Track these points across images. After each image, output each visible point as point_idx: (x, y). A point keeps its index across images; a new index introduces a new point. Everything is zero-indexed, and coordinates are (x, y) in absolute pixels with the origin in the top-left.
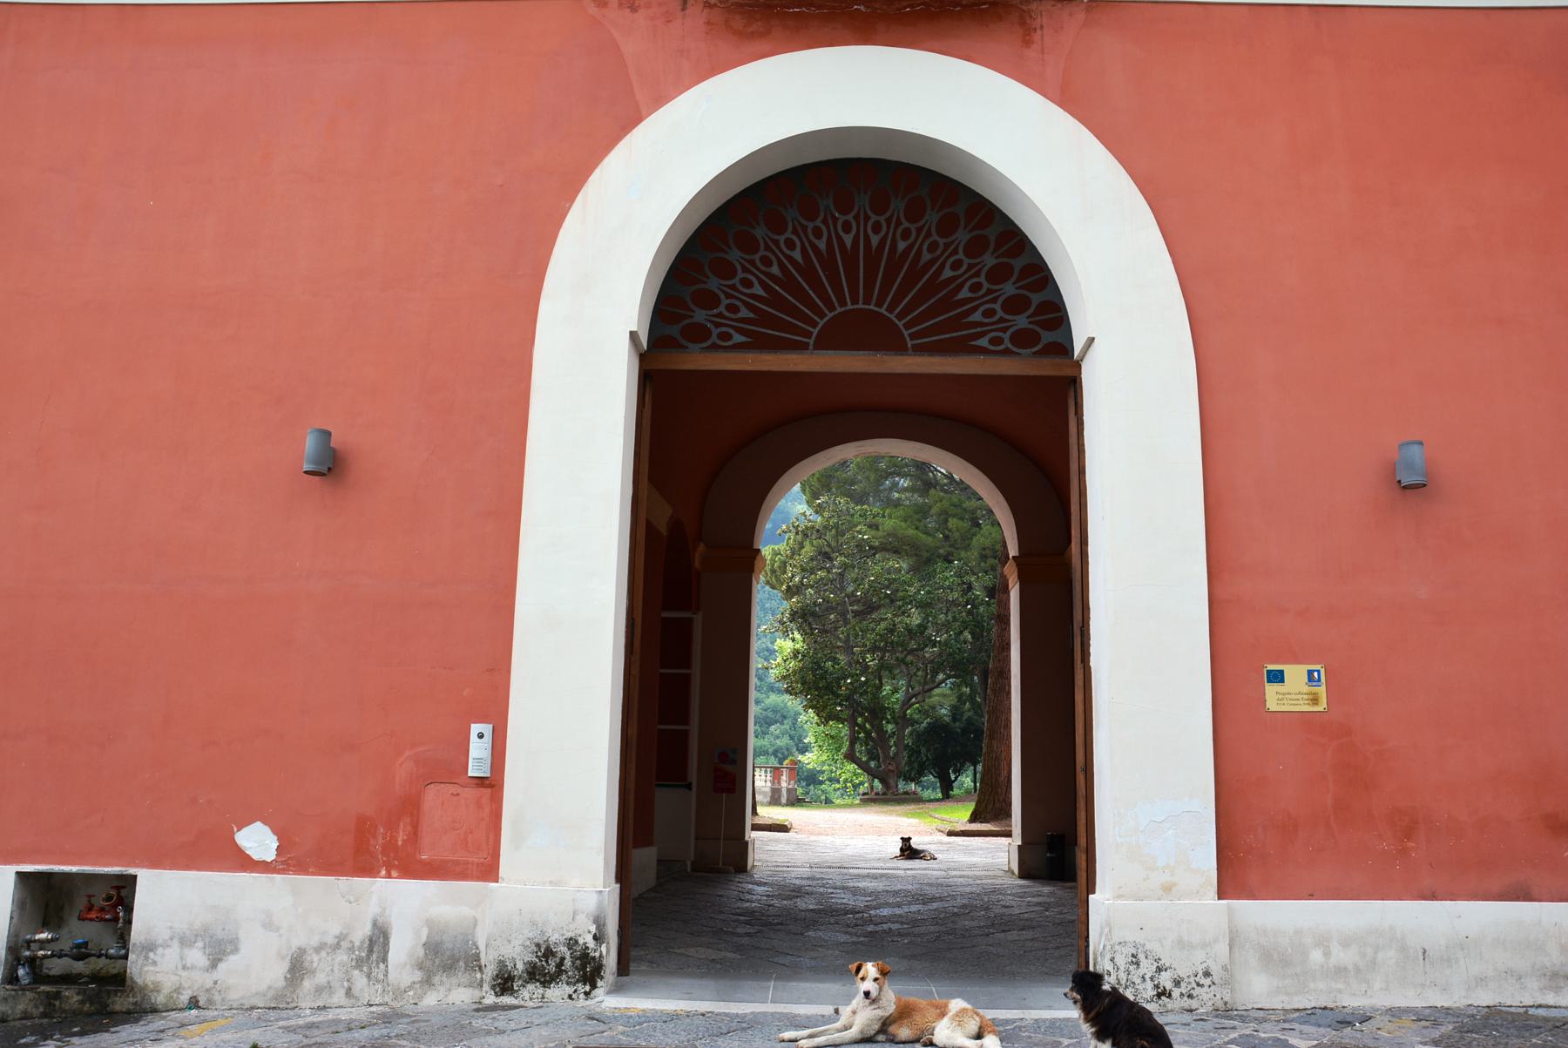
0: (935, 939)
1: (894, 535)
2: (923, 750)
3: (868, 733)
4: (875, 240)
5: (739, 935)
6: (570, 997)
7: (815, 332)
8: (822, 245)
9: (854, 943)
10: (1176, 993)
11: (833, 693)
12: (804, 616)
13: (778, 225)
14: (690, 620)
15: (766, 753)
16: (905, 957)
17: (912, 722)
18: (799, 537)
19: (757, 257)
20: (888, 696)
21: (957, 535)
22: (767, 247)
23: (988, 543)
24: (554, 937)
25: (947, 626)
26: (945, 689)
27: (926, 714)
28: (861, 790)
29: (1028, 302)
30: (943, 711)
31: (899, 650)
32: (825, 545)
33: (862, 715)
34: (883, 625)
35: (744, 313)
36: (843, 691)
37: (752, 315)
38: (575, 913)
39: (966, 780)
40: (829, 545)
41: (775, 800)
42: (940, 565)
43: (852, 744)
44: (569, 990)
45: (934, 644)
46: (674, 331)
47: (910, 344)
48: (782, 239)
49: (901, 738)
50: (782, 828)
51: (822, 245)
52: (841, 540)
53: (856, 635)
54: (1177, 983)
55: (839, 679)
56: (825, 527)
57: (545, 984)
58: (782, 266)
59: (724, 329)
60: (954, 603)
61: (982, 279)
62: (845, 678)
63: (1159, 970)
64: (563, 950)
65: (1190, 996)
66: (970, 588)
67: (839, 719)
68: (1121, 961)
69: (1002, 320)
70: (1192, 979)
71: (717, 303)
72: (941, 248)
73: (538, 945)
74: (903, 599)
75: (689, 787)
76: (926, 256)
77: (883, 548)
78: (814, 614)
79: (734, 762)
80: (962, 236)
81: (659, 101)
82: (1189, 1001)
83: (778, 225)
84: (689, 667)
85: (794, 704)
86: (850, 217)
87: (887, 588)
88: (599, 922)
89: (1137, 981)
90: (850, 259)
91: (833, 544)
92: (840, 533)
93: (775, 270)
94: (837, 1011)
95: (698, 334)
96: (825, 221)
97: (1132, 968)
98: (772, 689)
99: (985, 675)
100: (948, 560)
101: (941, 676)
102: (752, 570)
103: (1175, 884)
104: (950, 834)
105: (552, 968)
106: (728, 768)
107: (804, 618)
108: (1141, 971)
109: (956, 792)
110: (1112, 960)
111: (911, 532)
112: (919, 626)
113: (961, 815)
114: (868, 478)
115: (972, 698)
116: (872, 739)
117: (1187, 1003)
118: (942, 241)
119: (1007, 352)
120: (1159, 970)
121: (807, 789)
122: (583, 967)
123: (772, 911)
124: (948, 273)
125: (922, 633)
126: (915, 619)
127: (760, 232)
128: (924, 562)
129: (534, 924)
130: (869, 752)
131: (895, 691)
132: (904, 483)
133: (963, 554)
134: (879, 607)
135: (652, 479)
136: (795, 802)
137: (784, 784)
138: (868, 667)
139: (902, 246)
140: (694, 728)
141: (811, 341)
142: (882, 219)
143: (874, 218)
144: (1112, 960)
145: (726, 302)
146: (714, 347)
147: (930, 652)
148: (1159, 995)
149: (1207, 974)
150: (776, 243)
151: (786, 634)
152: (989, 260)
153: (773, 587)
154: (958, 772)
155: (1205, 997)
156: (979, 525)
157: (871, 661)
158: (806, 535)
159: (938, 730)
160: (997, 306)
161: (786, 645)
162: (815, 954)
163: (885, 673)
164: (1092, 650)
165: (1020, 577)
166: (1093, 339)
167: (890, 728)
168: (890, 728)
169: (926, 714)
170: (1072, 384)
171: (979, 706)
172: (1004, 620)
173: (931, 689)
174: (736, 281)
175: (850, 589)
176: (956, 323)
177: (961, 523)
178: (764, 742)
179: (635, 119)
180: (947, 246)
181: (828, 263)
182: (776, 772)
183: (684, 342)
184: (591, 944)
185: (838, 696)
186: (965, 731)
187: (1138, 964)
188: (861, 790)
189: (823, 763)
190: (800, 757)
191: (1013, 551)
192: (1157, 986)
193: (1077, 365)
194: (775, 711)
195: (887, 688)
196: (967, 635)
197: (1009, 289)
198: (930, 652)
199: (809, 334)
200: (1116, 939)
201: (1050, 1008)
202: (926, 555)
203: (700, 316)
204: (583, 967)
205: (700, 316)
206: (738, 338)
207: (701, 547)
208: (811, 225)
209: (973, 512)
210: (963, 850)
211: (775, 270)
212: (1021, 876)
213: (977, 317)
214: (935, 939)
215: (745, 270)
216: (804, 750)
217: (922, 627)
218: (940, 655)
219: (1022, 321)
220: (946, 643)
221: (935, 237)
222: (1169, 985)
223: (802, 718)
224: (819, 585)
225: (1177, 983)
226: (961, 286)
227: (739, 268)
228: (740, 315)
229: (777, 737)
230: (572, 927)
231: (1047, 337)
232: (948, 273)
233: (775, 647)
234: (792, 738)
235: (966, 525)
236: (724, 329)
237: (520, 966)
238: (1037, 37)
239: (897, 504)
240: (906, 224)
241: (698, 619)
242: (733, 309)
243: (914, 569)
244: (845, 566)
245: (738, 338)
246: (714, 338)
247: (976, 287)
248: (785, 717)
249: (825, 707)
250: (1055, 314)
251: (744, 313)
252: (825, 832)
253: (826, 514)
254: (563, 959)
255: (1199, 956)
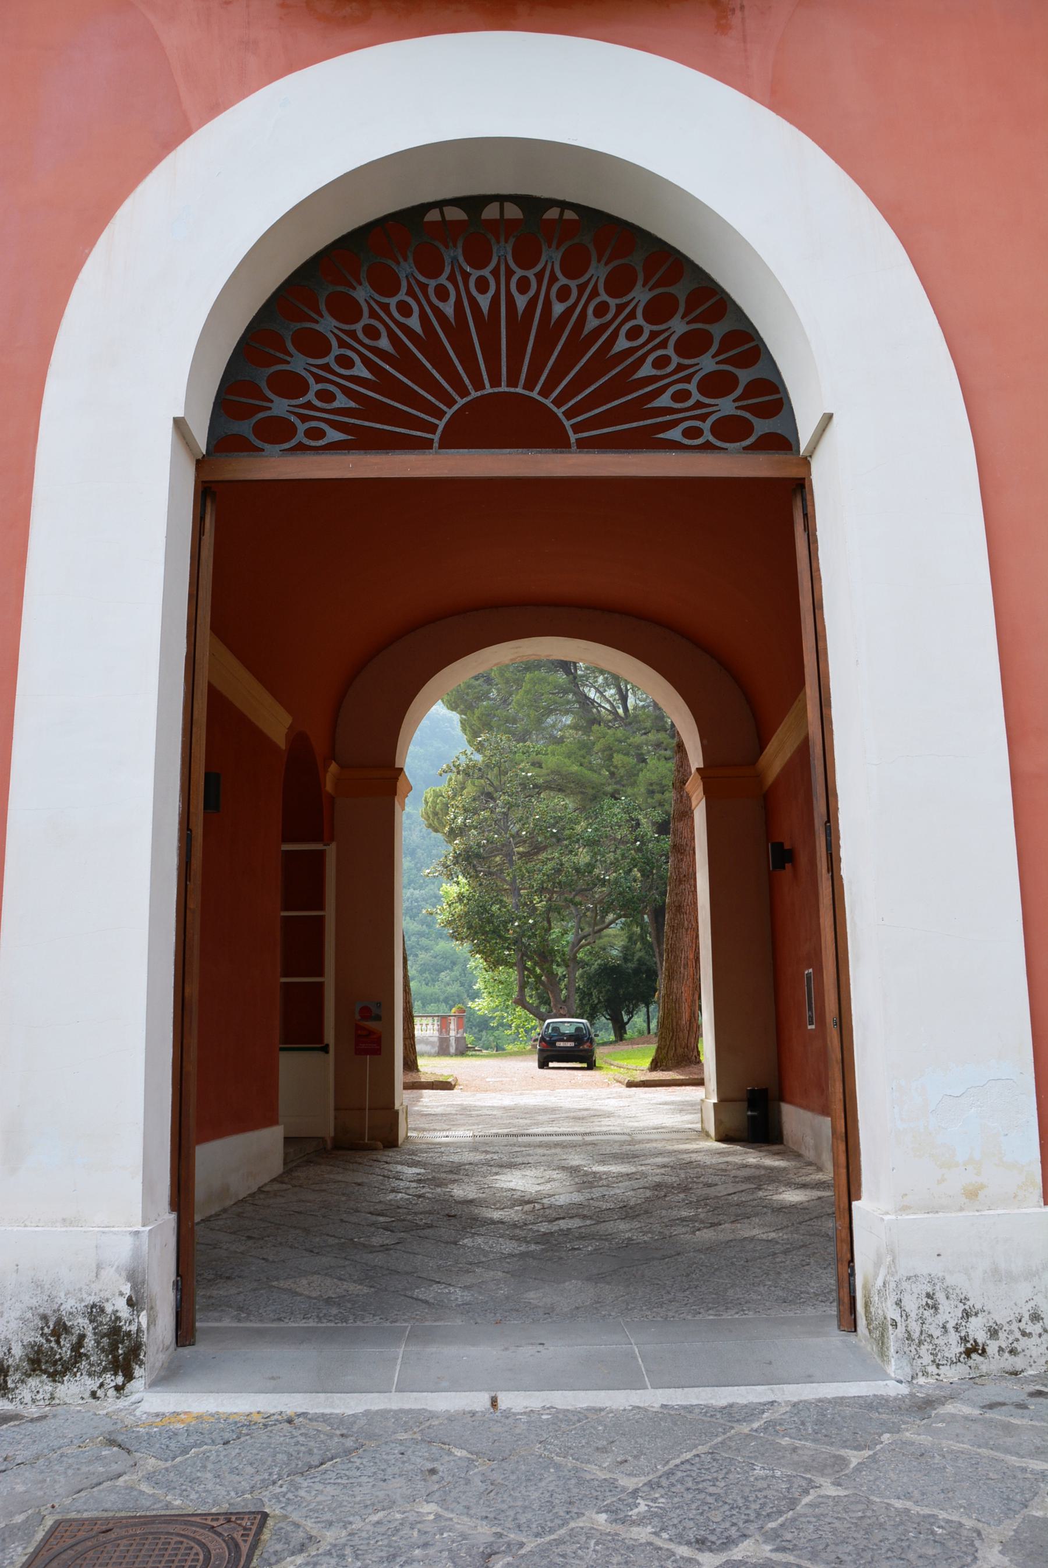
0: (624, 1250)
1: (558, 773)
2: (595, 992)
3: (538, 978)
4: (521, 302)
5: (372, 1250)
6: (94, 1395)
7: (441, 424)
8: (448, 309)
9: (523, 1255)
10: (992, 1348)
11: (500, 937)
12: (467, 858)
13: (387, 284)
14: (321, 854)
15: (437, 1000)
16: (589, 1279)
17: (583, 964)
18: (460, 777)
19: (358, 327)
20: (557, 940)
21: (622, 771)
22: (373, 314)
23: (654, 778)
24: (69, 1305)
25: (615, 864)
26: (614, 930)
27: (597, 955)
28: (534, 1034)
29: (734, 381)
30: (615, 952)
31: (567, 890)
32: (485, 784)
33: (531, 959)
34: (550, 865)
35: (342, 401)
36: (510, 934)
37: (352, 404)
38: (99, 1267)
39: (638, 1020)
40: (491, 784)
41: (443, 1050)
42: (607, 801)
43: (522, 988)
44: (92, 1384)
45: (603, 883)
46: (245, 428)
47: (573, 437)
48: (393, 302)
49: (572, 981)
50: (445, 1086)
51: (448, 309)
52: (504, 779)
53: (522, 877)
54: (993, 1333)
55: (505, 923)
56: (487, 766)
57: (55, 1376)
58: (393, 337)
59: (314, 424)
60: (622, 841)
61: (670, 351)
62: (512, 921)
63: (967, 1315)
64: (82, 1323)
65: (1013, 1352)
66: (638, 824)
67: (504, 962)
68: (911, 1305)
69: (699, 405)
70: (1014, 1326)
71: (305, 389)
72: (613, 311)
73: (44, 1318)
74: (569, 838)
75: (325, 1049)
76: (592, 323)
77: (548, 787)
78: (478, 856)
79: (378, 1018)
80: (641, 295)
81: (215, 108)
82: (1012, 1359)
83: (387, 284)
84: (321, 907)
85: (462, 948)
86: (486, 272)
87: (553, 826)
88: (135, 1277)
89: (937, 1332)
90: (488, 326)
91: (496, 783)
92: (503, 773)
93: (384, 343)
94: (494, 1402)
95: (277, 431)
96: (452, 278)
97: (927, 1314)
98: (440, 936)
99: (658, 914)
100: (614, 796)
101: (611, 916)
102: (394, 793)
103: (982, 1187)
104: (631, 1085)
105: (65, 1351)
106: (371, 1025)
107: (469, 861)
108: (941, 1318)
109: (630, 1033)
110: (899, 1303)
111: (575, 768)
112: (588, 865)
113: (638, 1061)
114: (528, 715)
115: (642, 938)
116: (542, 983)
117: (1009, 1362)
118: (613, 302)
119: (707, 447)
120: (967, 1315)
121: (477, 1038)
122: (113, 1347)
123: (423, 1205)
124: (622, 344)
125: (590, 872)
126: (583, 856)
127: (362, 294)
128: (591, 797)
129: (38, 1285)
130: (540, 997)
131: (565, 932)
132: (568, 720)
133: (629, 791)
134: (545, 848)
135: (218, 628)
136: (463, 1051)
137: (452, 1033)
138: (535, 909)
139: (558, 308)
140: (329, 979)
141: (436, 437)
142: (530, 274)
143: (519, 273)
144: (899, 1303)
145: (315, 387)
146: (301, 448)
147: (599, 892)
148: (968, 1353)
149: (1036, 1317)
150: (385, 307)
151: (450, 876)
152: (678, 326)
153: (436, 831)
154: (631, 1014)
155: (1035, 1352)
156: (644, 761)
157: (540, 904)
158: (467, 775)
159: (609, 974)
160: (692, 387)
161: (451, 890)
162: (468, 1279)
163: (553, 915)
164: (843, 853)
165: (706, 792)
166: (828, 418)
167: (560, 971)
168: (560, 971)
169: (597, 955)
170: (796, 490)
171: (650, 945)
172: (683, 850)
173: (602, 930)
174: (330, 359)
175: (514, 828)
176: (637, 410)
177: (626, 759)
178: (435, 989)
179: (183, 132)
180: (620, 308)
181: (458, 332)
182: (444, 1021)
183: (258, 443)
184: (125, 1312)
185: (506, 939)
186: (637, 971)
187: (935, 1307)
188: (534, 1034)
189: (495, 1009)
190: (470, 1004)
191: (696, 760)
192: (964, 1339)
193: (806, 462)
194: (445, 957)
195: (556, 931)
196: (636, 873)
197: (707, 363)
198: (599, 892)
199: (433, 428)
200: (902, 1272)
201: (809, 1379)
202: (590, 791)
203: (281, 407)
204: (113, 1347)
205: (281, 407)
206: (334, 435)
207: (333, 767)
208: (432, 284)
209: (639, 747)
210: (645, 1109)
211: (384, 343)
212: (721, 1139)
213: (664, 401)
214: (624, 1250)
215: (342, 344)
216: (475, 996)
217: (591, 866)
218: (610, 894)
219: (726, 406)
220: (616, 881)
221: (604, 297)
222: (981, 1337)
223: (472, 964)
224: (479, 827)
225: (993, 1333)
226: (642, 360)
227: (334, 343)
228: (336, 404)
229: (447, 983)
230: (96, 1287)
231: (762, 426)
232: (622, 344)
233: (428, 886)
234: (462, 985)
235: (633, 761)
236: (314, 424)
237: (18, 1351)
238: (735, 20)
239: (560, 741)
240: (563, 280)
241: (331, 851)
242: (326, 396)
243: (582, 809)
244: (510, 806)
245: (334, 435)
246: (300, 437)
247: (661, 362)
248: (454, 963)
249: (492, 952)
250: (770, 397)
251: (342, 401)
252: (490, 1096)
253: (488, 753)
254: (82, 1337)
255: (1023, 1290)
